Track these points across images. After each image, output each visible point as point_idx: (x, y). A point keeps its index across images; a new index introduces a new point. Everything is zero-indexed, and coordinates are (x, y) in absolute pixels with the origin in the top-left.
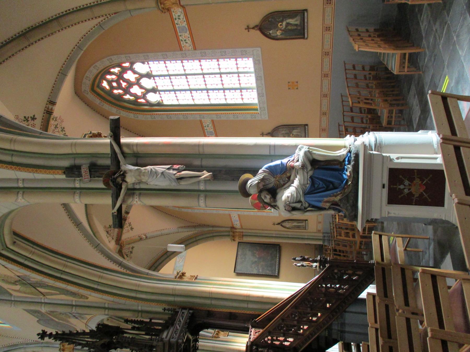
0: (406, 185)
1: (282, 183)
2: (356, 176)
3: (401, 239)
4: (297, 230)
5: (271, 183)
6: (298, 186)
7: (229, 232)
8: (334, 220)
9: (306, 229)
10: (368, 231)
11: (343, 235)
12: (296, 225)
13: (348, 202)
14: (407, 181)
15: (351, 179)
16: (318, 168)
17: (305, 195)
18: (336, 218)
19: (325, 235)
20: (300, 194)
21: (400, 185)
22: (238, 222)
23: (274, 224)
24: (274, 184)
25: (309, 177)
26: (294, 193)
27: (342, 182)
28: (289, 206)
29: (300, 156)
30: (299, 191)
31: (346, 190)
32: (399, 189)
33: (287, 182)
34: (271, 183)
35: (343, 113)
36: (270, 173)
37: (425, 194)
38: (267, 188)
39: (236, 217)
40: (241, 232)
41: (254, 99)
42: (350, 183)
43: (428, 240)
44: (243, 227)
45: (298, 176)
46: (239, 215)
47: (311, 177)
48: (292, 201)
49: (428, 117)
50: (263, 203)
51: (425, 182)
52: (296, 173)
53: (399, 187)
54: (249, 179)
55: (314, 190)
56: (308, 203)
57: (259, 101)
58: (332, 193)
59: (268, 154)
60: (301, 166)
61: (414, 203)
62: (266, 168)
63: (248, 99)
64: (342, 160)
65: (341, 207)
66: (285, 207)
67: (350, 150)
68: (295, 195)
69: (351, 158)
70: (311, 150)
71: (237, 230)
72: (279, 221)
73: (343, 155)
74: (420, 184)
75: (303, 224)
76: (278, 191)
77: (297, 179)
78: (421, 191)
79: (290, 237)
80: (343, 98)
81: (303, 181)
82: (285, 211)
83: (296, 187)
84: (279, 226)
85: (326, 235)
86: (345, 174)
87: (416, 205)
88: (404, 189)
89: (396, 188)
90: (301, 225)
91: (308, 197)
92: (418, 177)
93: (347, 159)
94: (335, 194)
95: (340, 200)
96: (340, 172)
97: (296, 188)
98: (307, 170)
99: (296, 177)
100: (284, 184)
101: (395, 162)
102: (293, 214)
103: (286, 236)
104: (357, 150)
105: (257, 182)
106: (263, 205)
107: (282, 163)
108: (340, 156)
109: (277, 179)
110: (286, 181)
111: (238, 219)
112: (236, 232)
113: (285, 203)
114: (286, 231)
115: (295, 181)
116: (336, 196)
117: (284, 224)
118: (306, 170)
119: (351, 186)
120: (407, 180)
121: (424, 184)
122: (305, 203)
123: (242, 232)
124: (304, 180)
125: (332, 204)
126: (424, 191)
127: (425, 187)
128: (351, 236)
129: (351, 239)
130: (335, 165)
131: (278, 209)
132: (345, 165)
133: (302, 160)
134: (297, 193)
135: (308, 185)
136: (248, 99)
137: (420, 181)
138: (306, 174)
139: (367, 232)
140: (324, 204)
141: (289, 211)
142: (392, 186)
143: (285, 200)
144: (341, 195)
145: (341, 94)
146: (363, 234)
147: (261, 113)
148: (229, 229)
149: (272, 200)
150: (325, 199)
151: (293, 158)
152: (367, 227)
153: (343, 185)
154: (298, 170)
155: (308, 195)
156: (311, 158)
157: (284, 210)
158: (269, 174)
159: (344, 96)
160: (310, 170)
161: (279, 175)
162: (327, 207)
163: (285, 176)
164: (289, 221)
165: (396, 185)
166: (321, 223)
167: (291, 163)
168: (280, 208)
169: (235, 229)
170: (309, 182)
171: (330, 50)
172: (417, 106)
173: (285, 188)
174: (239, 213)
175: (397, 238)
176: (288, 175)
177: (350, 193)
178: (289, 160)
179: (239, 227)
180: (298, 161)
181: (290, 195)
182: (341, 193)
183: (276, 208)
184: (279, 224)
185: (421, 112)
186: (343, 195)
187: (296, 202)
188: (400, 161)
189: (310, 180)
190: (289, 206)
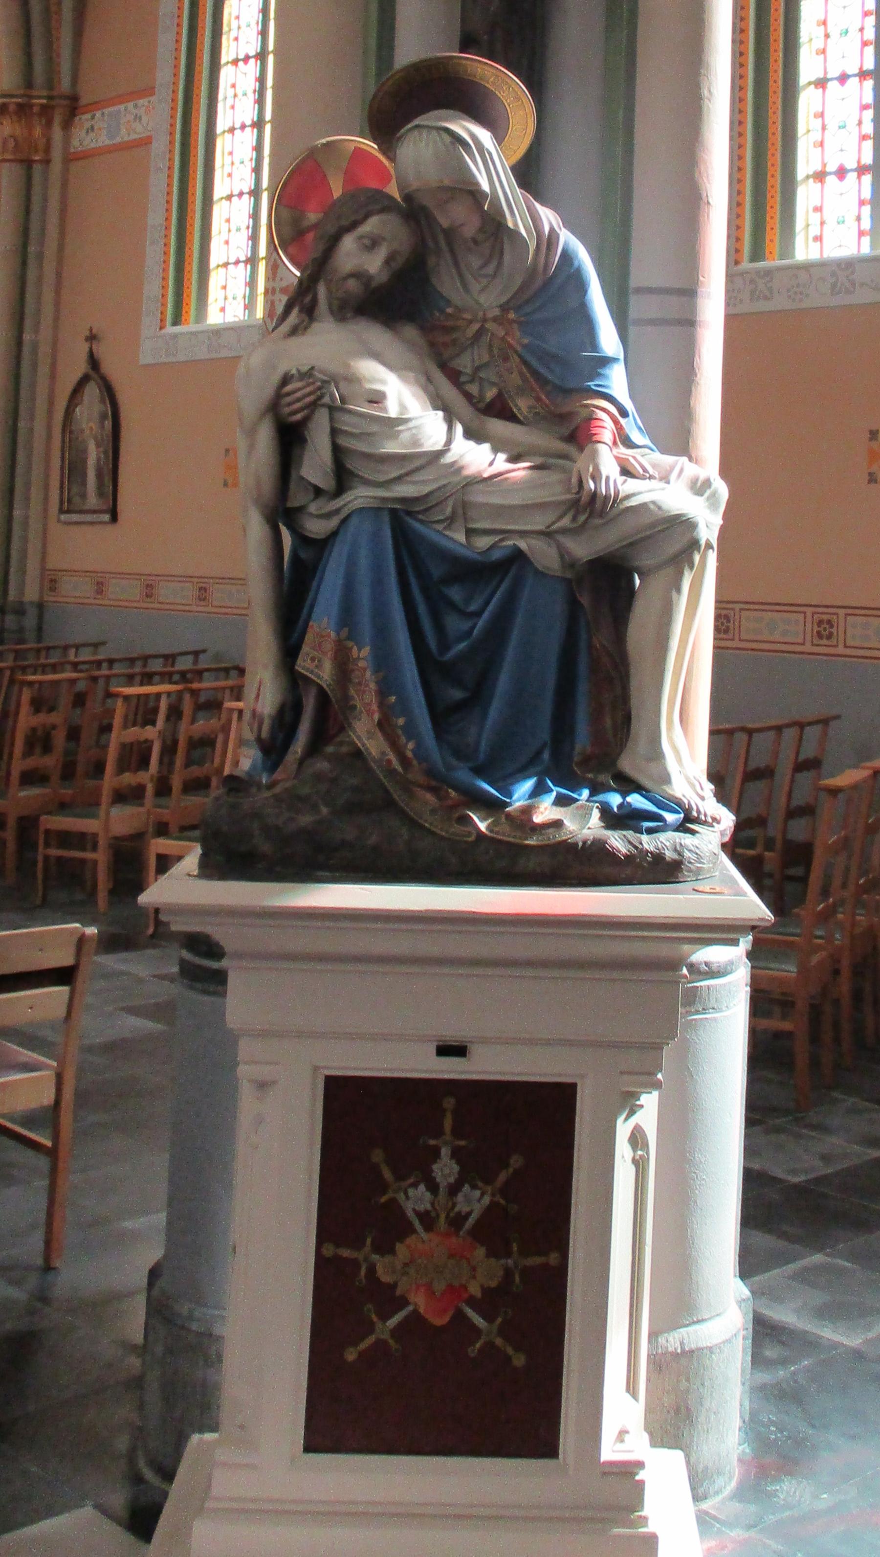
0: (460, 1197)
1: (465, 363)
2: (531, 864)
3: (47, 1097)
4: (56, 462)
5: (465, 285)
6: (456, 468)
7: (51, 83)
8: (118, 669)
9: (61, 511)
10: (59, 859)
11: (42, 718)
12: (84, 461)
13: (351, 809)
14: (487, 1200)
15: (506, 834)
16: (574, 605)
17: (393, 512)
18: (130, 679)
19: (32, 613)
20: (399, 479)
21: (456, 1154)
22: (103, 140)
23: (92, 338)
24: (458, 309)
25: (522, 545)
26: (405, 437)
27: (480, 771)
28: (314, 406)
29: (654, 484)
30: (417, 477)
31: (429, 797)
32: (435, 1154)
33: (468, 396)
34: (465, 285)
35: (743, 729)
36: (539, 282)
37: (393, 1322)
38: (431, 261)
39: (138, 127)
40: (48, 149)
41: (819, 239)
42: (482, 826)
43: (40, 1261)
44: (74, 167)
45: (520, 471)
46: (146, 142)
47: (518, 557)
48: (346, 423)
49: (782, 1235)
50: (331, 229)
51: (479, 1321)
52: (539, 460)
53: (445, 1152)
54: (499, 137)
55: (423, 575)
56: (334, 534)
57: (807, 267)
58: (404, 707)
59: (634, 281)
60: (594, 496)
61: (329, 1250)
62: (567, 257)
63: (818, 209)
64: (626, 764)
65: (301, 762)
66: (308, 374)
67: (696, 821)
68: (391, 448)
69: (650, 831)
70: (697, 558)
71: (57, 133)
72: (111, 367)
73: (666, 779)
74: (464, 1288)
75: (93, 500)
76: (410, 331)
77: (501, 463)
78: (419, 1301)
79: (21, 424)
80: (816, 730)
81: (496, 500)
82: (276, 379)
83: (448, 458)
84: (81, 367)
85: (30, 622)
86: (539, 791)
87: (321, 1263)
88: (433, 1187)
89: (438, 1133)
90: (84, 484)
91: (376, 537)
92: (508, 1274)
93: (636, 800)
94: (401, 721)
95: (358, 754)
96: (546, 755)
97: (440, 454)
98: (564, 531)
99: (514, 458)
100: (454, 376)
101: (620, 1121)
102: (251, 433)
103: (23, 406)
104: (699, 870)
105: (485, 186)
106: (315, 226)
107: (606, 361)
108: (657, 755)
109: (489, 325)
110: (474, 389)
111: (124, 136)
112: (49, 123)
113: (334, 379)
114: (51, 403)
115: (486, 447)
116: (383, 725)
117: (92, 391)
118: (566, 522)
119: (457, 828)
120: (493, 1205)
121: (460, 1316)
122: (328, 516)
123: (47, 162)
124: (500, 511)
125: (323, 696)
126: (415, 1312)
127: (439, 1321)
128: (31, 762)
129: (18, 766)
130: (596, 717)
131: (286, 327)
132: (595, 790)
133: (633, 502)
134: (402, 458)
135: (461, 537)
136: (818, 209)
137: (485, 1290)
138: (538, 522)
139: (54, 852)
140: (329, 646)
141: (274, 407)
142: (449, 1103)
143: (353, 379)
144: (396, 765)
145: (837, 717)
146: (47, 832)
147: (742, 274)
148: (65, 84)
149: (352, 285)
150: (363, 654)
151: (636, 437)
152: (89, 855)
153: (463, 775)
154: (567, 471)
155: (387, 533)
156: (646, 560)
157: (283, 367)
158: (532, 272)
159: (825, 734)
160: (563, 553)
161: (518, 339)
162: (303, 665)
163: (515, 379)
164: (108, 424)
165: (457, 1132)
166: (100, 592)
167: (608, 423)
168: (295, 341)
169: (67, 125)
170: (483, 543)
171: (809, 615)
172: (826, 1158)
173: (429, 379)
174: (159, 145)
175: (48, 1075)
176: (522, 405)
177: (413, 824)
178: (624, 413)
179: (75, 142)
180: (626, 472)
181: (393, 411)
182: (405, 761)
183: (294, 317)
184: (94, 362)
185: (796, 1187)
186: (391, 772)
187: (337, 451)
188: (623, 1151)
189: (496, 555)
190: (314, 406)
